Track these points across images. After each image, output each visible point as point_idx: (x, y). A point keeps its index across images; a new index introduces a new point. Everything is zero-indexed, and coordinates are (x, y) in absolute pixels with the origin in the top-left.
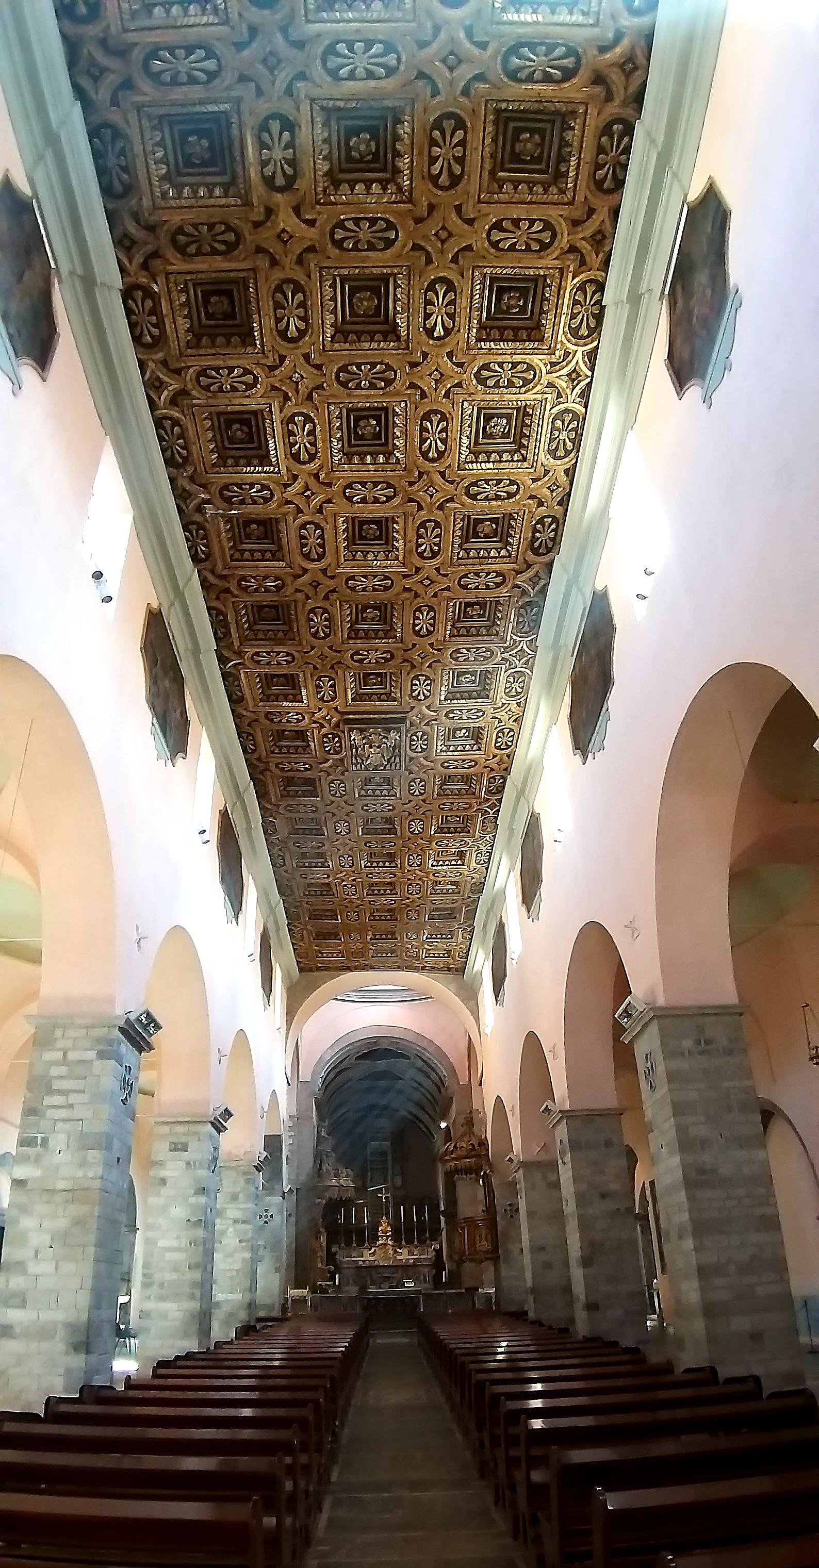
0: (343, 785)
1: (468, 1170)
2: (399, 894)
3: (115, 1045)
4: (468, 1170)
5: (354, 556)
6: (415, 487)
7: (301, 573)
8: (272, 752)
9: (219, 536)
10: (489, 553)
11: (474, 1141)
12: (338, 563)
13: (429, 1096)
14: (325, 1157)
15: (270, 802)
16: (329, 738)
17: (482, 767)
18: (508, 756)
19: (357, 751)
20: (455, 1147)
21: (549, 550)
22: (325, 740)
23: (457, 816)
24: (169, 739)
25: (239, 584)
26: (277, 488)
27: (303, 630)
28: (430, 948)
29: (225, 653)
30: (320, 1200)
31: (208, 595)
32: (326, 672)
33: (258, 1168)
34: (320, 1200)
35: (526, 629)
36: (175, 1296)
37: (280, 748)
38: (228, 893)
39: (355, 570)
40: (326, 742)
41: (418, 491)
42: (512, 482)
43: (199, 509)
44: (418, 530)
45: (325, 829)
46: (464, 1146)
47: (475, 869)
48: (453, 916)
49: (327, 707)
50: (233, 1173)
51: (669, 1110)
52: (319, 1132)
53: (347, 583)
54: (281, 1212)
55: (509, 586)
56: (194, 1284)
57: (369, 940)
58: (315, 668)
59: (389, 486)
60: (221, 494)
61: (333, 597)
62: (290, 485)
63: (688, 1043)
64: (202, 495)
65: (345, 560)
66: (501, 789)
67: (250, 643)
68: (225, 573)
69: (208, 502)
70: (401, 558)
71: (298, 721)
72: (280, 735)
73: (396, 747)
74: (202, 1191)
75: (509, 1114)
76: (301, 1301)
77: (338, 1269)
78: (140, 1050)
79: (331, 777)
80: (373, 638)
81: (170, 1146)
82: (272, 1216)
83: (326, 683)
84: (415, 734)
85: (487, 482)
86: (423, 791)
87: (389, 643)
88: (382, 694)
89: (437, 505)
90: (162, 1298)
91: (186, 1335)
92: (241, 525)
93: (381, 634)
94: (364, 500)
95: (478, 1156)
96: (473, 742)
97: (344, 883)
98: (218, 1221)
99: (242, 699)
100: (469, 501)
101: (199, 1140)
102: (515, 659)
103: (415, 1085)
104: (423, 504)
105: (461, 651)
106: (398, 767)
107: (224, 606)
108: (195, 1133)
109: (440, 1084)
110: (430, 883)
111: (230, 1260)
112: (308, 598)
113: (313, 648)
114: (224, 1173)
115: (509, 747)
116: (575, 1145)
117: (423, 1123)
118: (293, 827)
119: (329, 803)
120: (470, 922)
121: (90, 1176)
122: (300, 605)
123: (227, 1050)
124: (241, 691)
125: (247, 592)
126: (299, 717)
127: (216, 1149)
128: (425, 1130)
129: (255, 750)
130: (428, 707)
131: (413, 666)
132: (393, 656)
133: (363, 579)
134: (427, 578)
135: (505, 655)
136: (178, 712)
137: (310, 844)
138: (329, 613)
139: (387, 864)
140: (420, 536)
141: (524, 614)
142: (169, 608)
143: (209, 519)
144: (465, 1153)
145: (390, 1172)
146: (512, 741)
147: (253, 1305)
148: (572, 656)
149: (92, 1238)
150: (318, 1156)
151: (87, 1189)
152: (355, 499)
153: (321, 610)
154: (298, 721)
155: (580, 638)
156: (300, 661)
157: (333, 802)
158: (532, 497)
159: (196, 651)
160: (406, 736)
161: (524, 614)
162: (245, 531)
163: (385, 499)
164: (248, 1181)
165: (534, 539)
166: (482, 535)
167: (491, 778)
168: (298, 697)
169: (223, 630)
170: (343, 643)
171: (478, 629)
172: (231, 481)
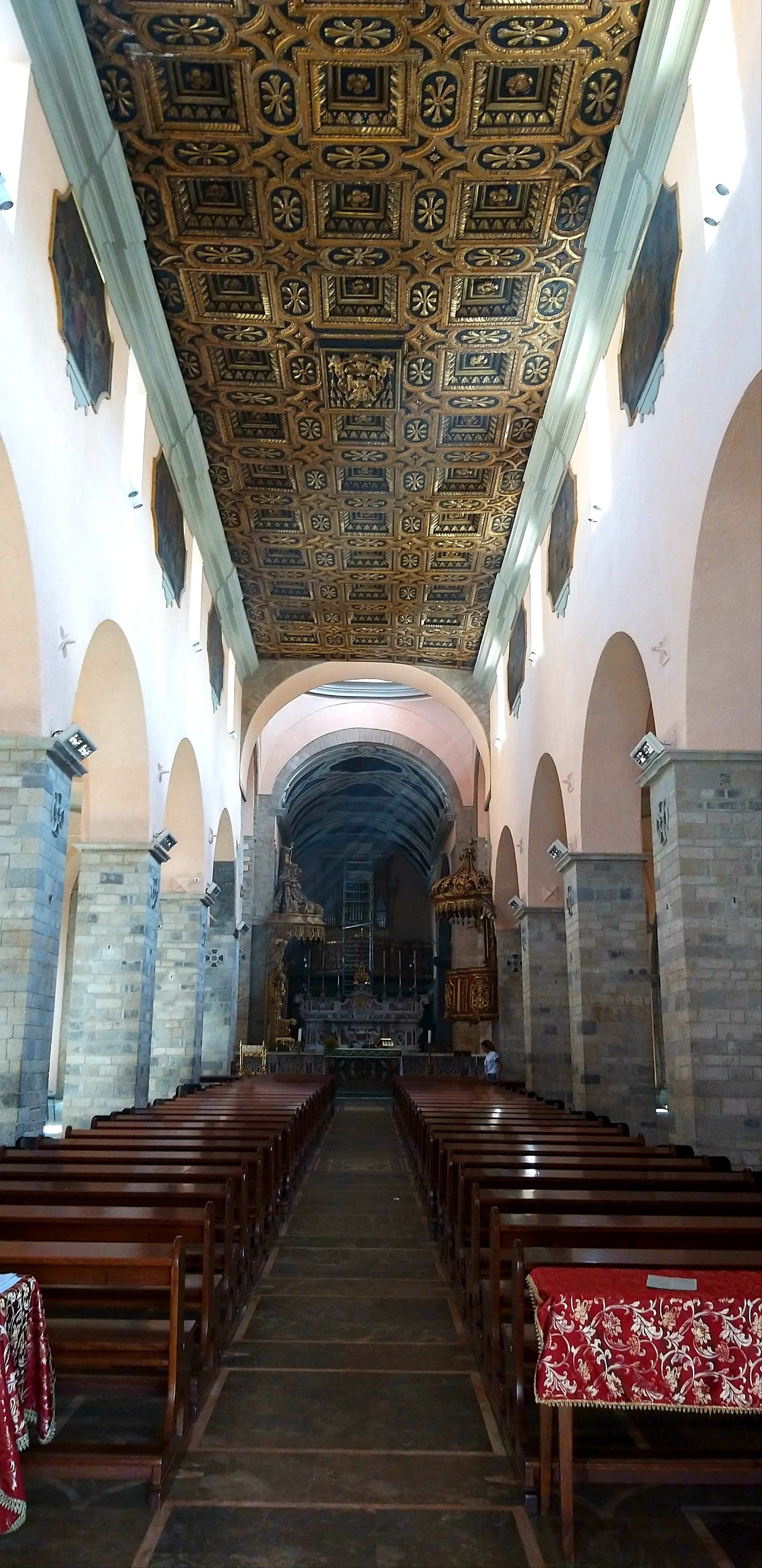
0: (317, 424)
1: (465, 912)
2: (390, 566)
3: (44, 770)
4: (465, 912)
5: (335, 118)
6: (421, 28)
7: (262, 140)
8: (222, 378)
9: (148, 86)
10: (522, 118)
11: (475, 878)
12: (313, 128)
13: (424, 818)
14: (288, 888)
15: (219, 442)
16: (299, 363)
17: (504, 405)
18: (541, 393)
19: (336, 381)
20: (451, 884)
21: (606, 117)
22: (294, 365)
23: (470, 470)
24: (88, 377)
25: (176, 152)
26: (229, 24)
27: (264, 220)
28: (429, 635)
29: (159, 245)
30: (281, 940)
31: (134, 168)
32: (296, 275)
33: (205, 903)
34: (281, 940)
35: (571, 223)
36: (109, 1049)
37: (234, 372)
38: (166, 568)
39: (336, 139)
40: (295, 368)
41: (425, 33)
42: (558, 24)
43: (120, 49)
44: (424, 87)
45: (293, 481)
46: (462, 883)
47: (491, 538)
48: (462, 595)
49: (296, 322)
50: (174, 908)
51: (676, 869)
52: (282, 859)
53: (324, 156)
54: (232, 954)
55: (549, 166)
56: (130, 1036)
57: (350, 622)
58: (281, 269)
59: (385, 24)
60: (150, 29)
61: (306, 174)
62: (247, 20)
63: (708, 794)
64: (125, 31)
65: (322, 124)
66: (529, 435)
67: (191, 232)
68: (158, 136)
69: (132, 39)
70: (399, 122)
71: (258, 338)
72: (233, 356)
73: (389, 378)
74: (141, 930)
75: (517, 850)
76: (256, 1059)
77: (301, 1023)
78: (71, 774)
79: (302, 414)
80: (361, 232)
81: (101, 877)
82: (221, 958)
83: (295, 293)
84: (415, 361)
85: (522, 22)
86: (423, 436)
87: (380, 239)
88: (370, 306)
89: (452, 51)
90: (91, 1051)
91: (120, 1093)
92: (179, 71)
93: (371, 225)
94: (349, 43)
95: (479, 896)
96: (492, 372)
97: (318, 551)
98: (157, 963)
99: (181, 307)
100: (496, 48)
101: (136, 871)
102: (553, 265)
103: (409, 805)
104: (432, 51)
105: (480, 252)
106: (391, 406)
107: (156, 181)
108: (130, 864)
109: (438, 805)
110: (431, 554)
111: (171, 1009)
112: (271, 174)
113: (278, 242)
114: (164, 908)
115: (541, 381)
116: (585, 895)
117: (416, 849)
118: (250, 475)
119: (299, 446)
120: (482, 605)
121: (20, 916)
122: (260, 185)
123: (168, 766)
124: (180, 296)
125: (188, 164)
126: (259, 333)
127: (156, 881)
128: (418, 858)
129: (200, 375)
130: (434, 327)
131: (414, 271)
132: (386, 257)
133: (347, 151)
134: (435, 152)
135: (539, 260)
136: (99, 334)
137: (274, 499)
138: (300, 197)
139: (375, 528)
140: (426, 95)
141: (569, 204)
142: (82, 188)
143: (136, 64)
144: (462, 891)
145: (371, 909)
146: (546, 374)
147: (197, 1063)
148: (630, 268)
149: (24, 983)
150: (280, 887)
151: (17, 931)
152: (337, 41)
153: (289, 193)
154: (258, 338)
155: (641, 245)
156: (260, 259)
157: (303, 447)
158: (584, 44)
159: (119, 245)
160: (403, 364)
161: (569, 204)
162: (184, 77)
163: (378, 42)
164: (193, 918)
165: (586, 102)
166: (514, 92)
167: (516, 421)
168: (258, 307)
169: (154, 214)
170: (319, 236)
171: (505, 221)
172: (165, 12)
